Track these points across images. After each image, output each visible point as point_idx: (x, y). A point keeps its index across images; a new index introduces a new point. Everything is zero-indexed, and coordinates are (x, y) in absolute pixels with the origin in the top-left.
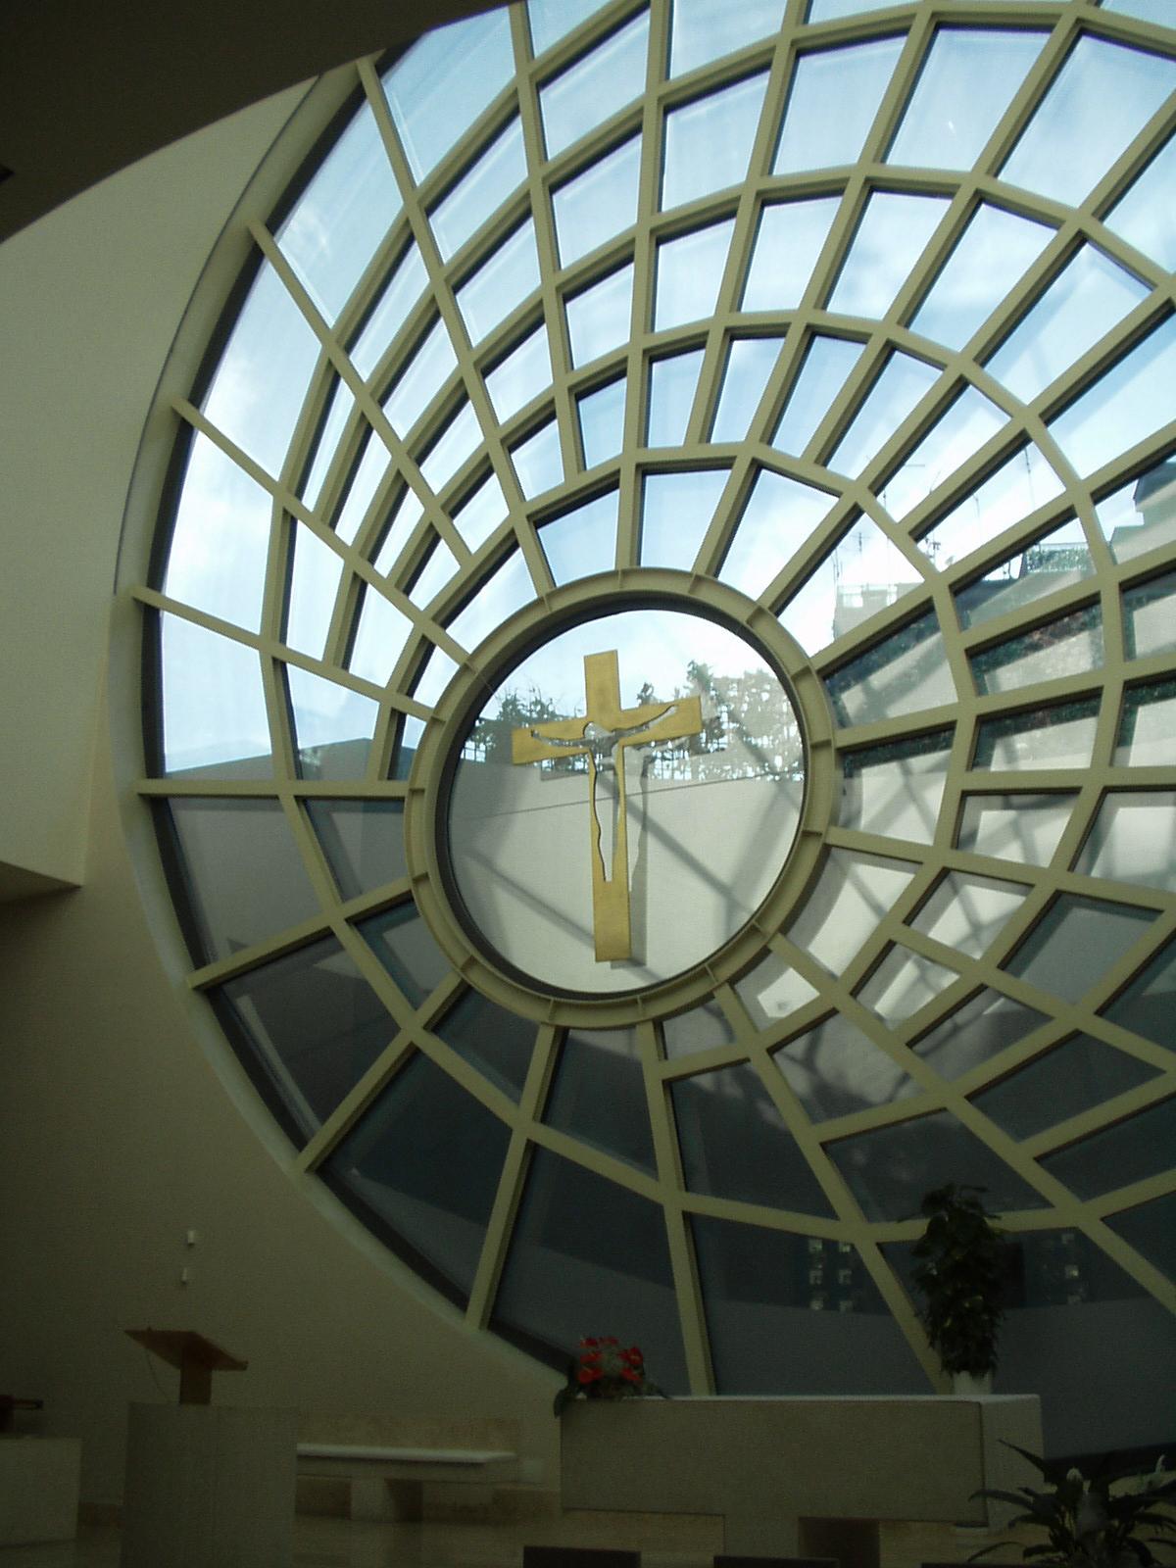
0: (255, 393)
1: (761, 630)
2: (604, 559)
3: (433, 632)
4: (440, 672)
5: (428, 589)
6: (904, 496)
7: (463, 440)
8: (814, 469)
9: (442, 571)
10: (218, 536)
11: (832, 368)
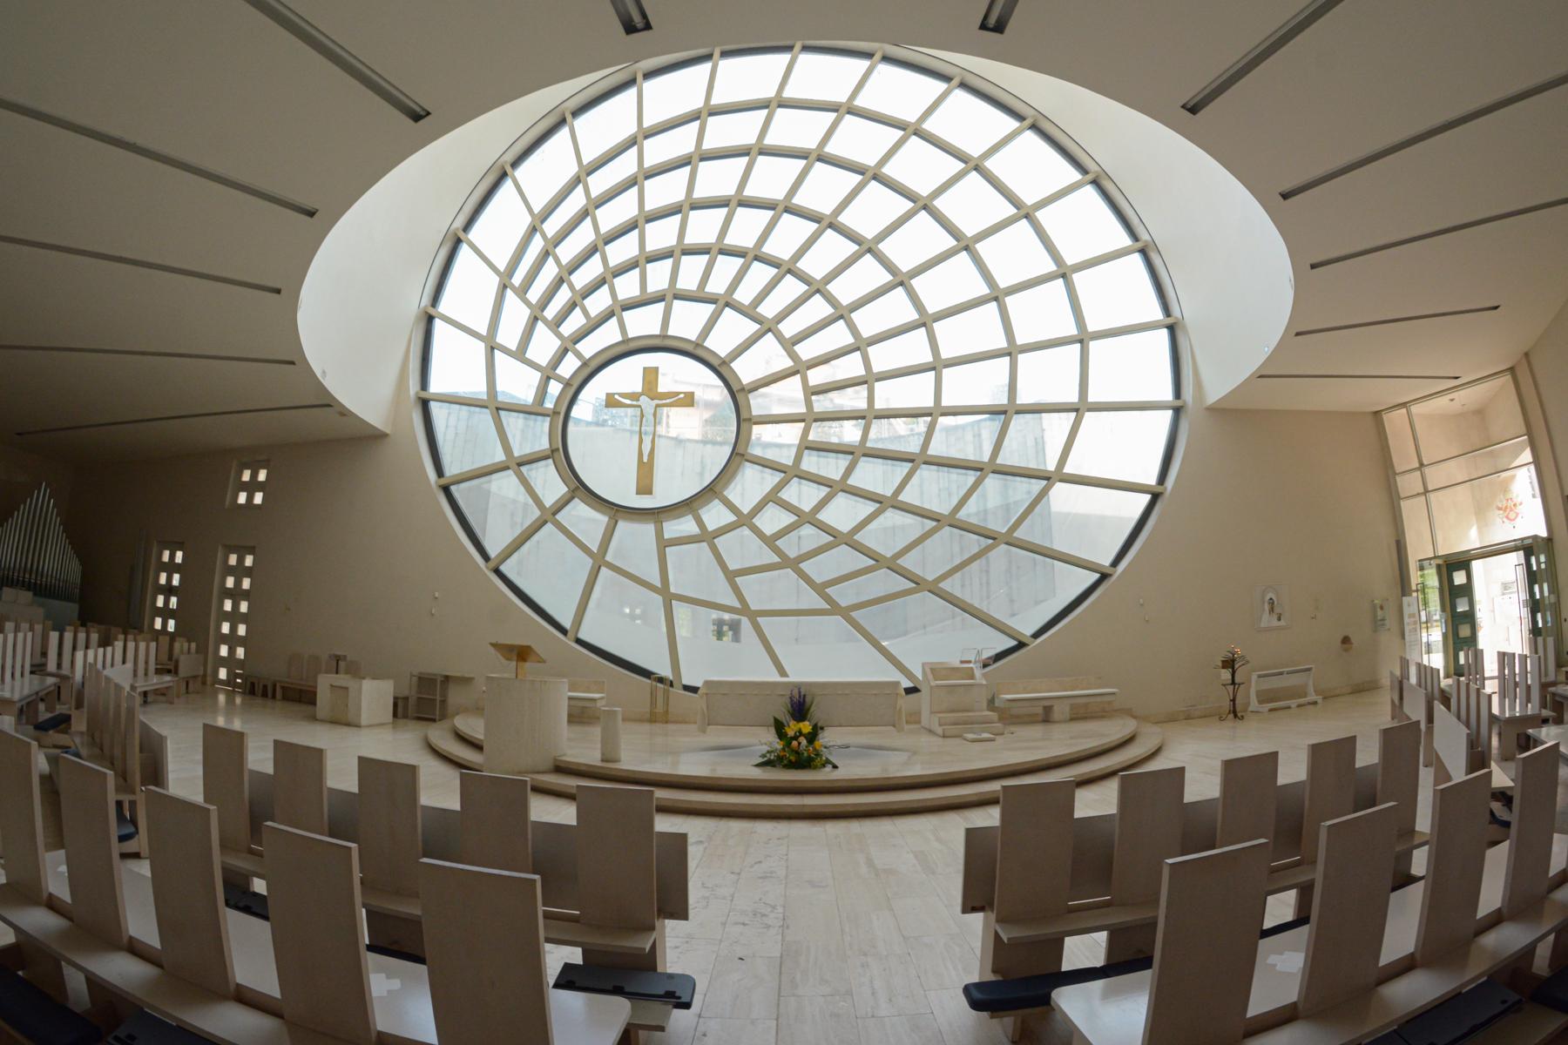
0: (500, 228)
2: (655, 330)
3: (578, 300)
7: (593, 268)
8: (789, 345)
9: (575, 321)
10: (470, 289)
11: (819, 308)
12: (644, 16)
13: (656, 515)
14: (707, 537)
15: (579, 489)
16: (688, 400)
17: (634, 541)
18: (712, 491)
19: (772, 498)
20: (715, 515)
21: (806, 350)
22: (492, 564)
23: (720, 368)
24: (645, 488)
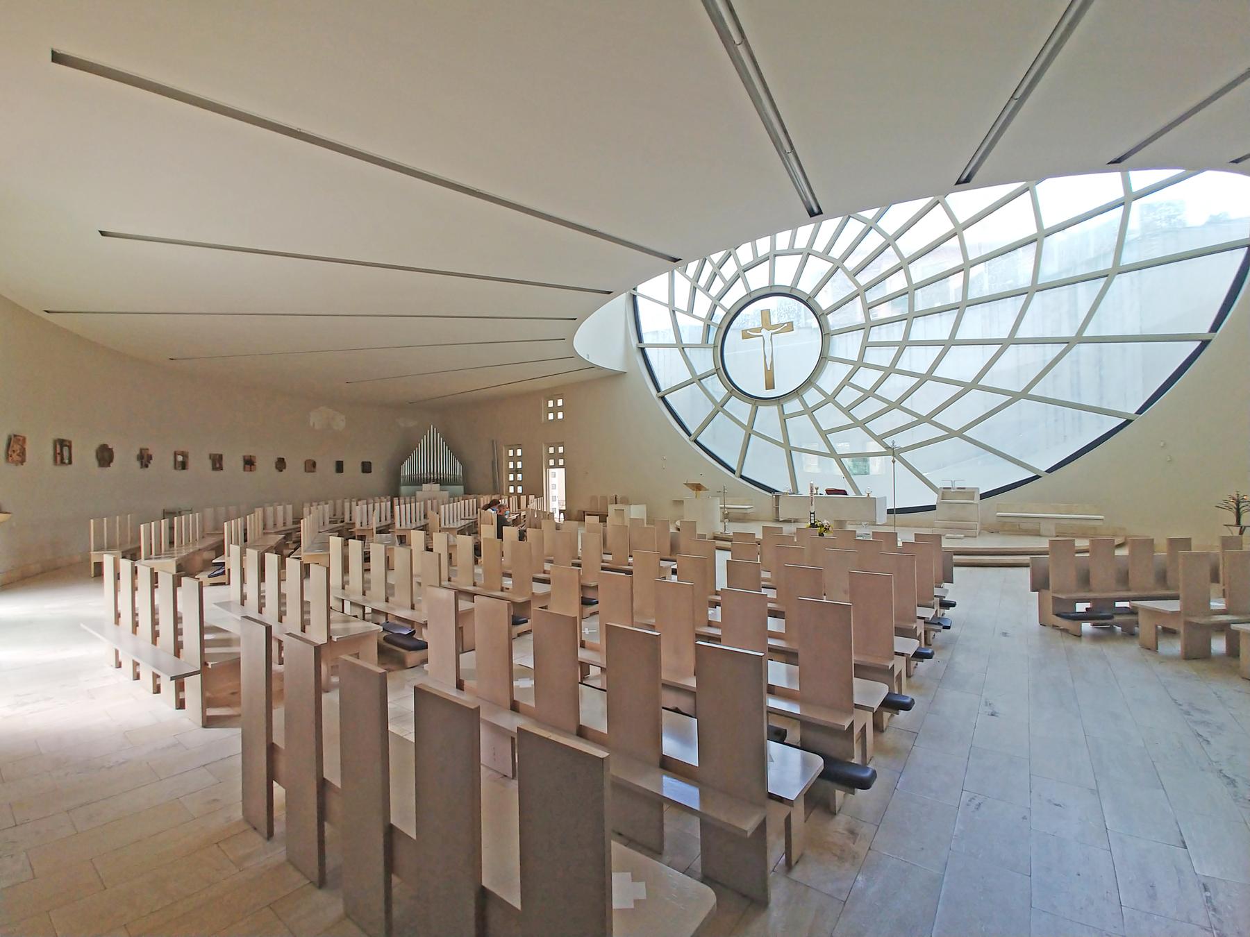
1: (810, 302)
4: (720, 313)
5: (714, 291)
6: (851, 263)
8: (825, 255)
9: (718, 285)
12: (819, 207)
13: (778, 400)
14: (810, 412)
15: (735, 390)
16: (789, 327)
17: (768, 417)
18: (809, 382)
19: (847, 382)
20: (812, 397)
21: (836, 253)
22: (692, 438)
23: (808, 302)
24: (770, 385)
